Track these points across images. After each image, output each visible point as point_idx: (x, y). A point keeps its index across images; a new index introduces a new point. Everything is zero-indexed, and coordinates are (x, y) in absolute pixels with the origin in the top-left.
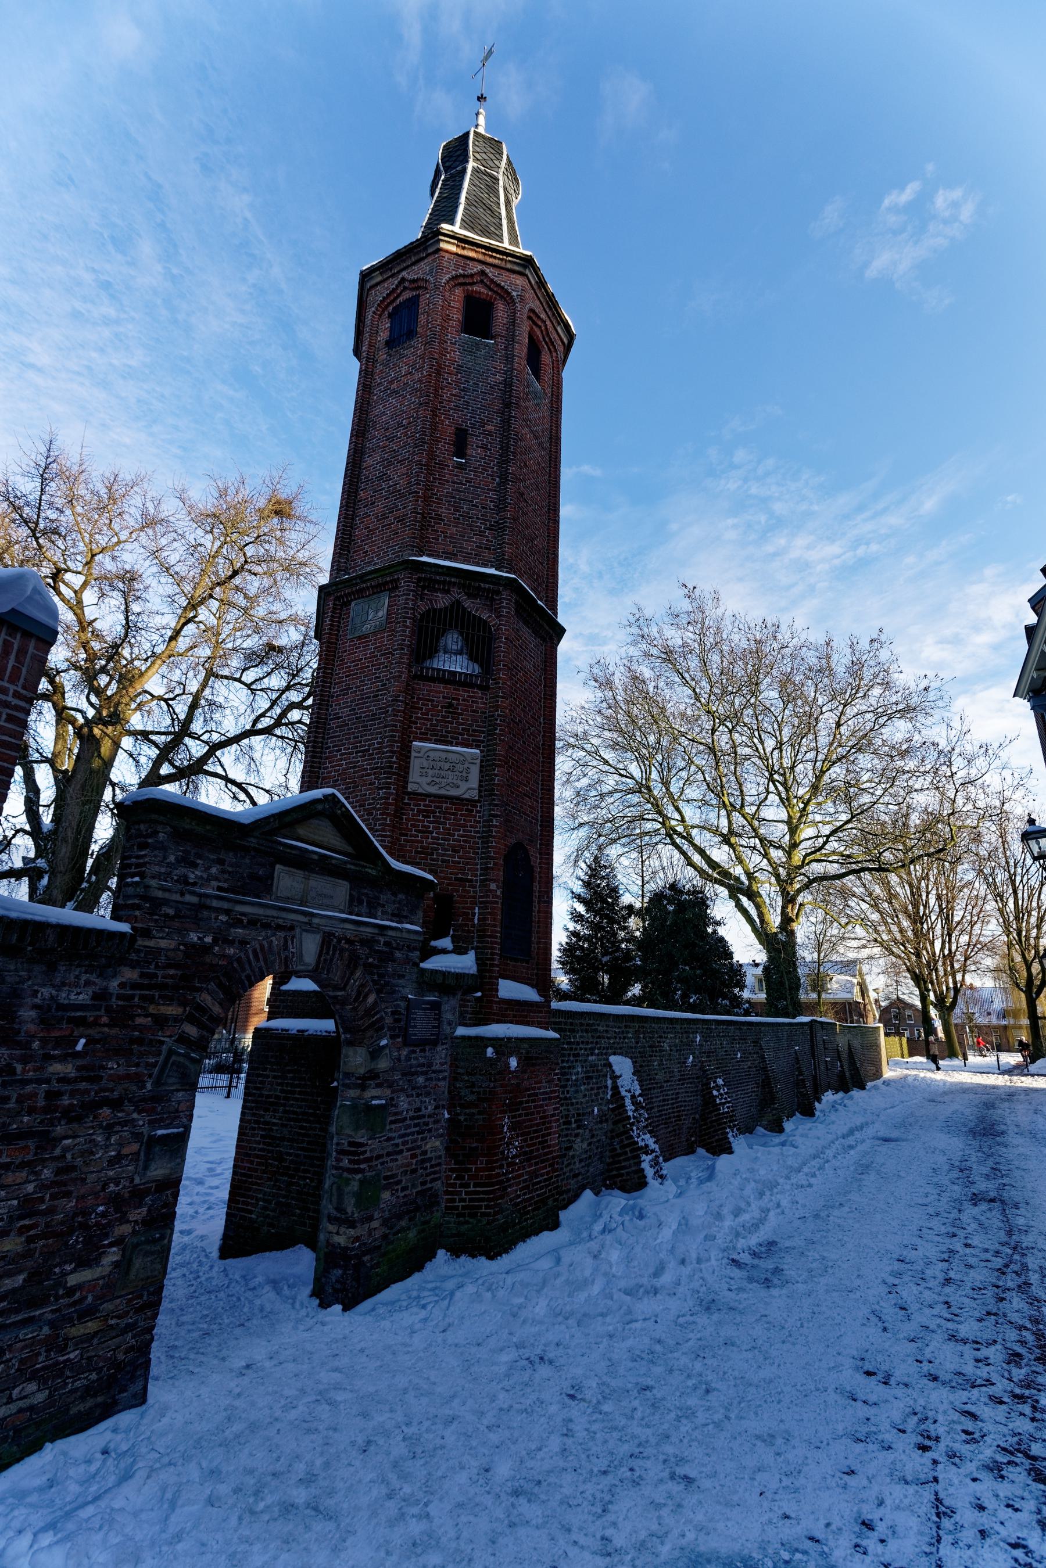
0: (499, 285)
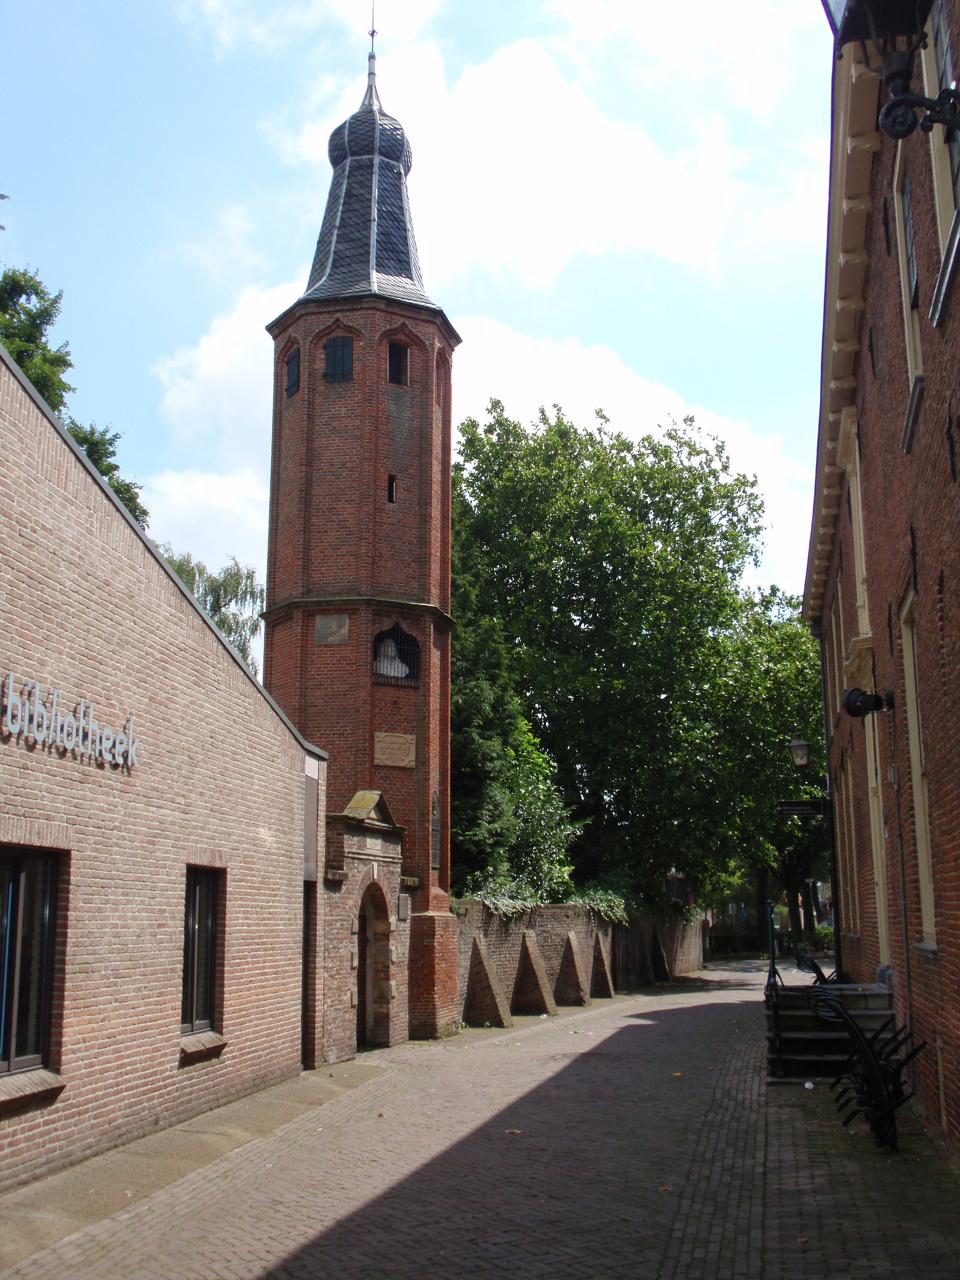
0: (416, 336)
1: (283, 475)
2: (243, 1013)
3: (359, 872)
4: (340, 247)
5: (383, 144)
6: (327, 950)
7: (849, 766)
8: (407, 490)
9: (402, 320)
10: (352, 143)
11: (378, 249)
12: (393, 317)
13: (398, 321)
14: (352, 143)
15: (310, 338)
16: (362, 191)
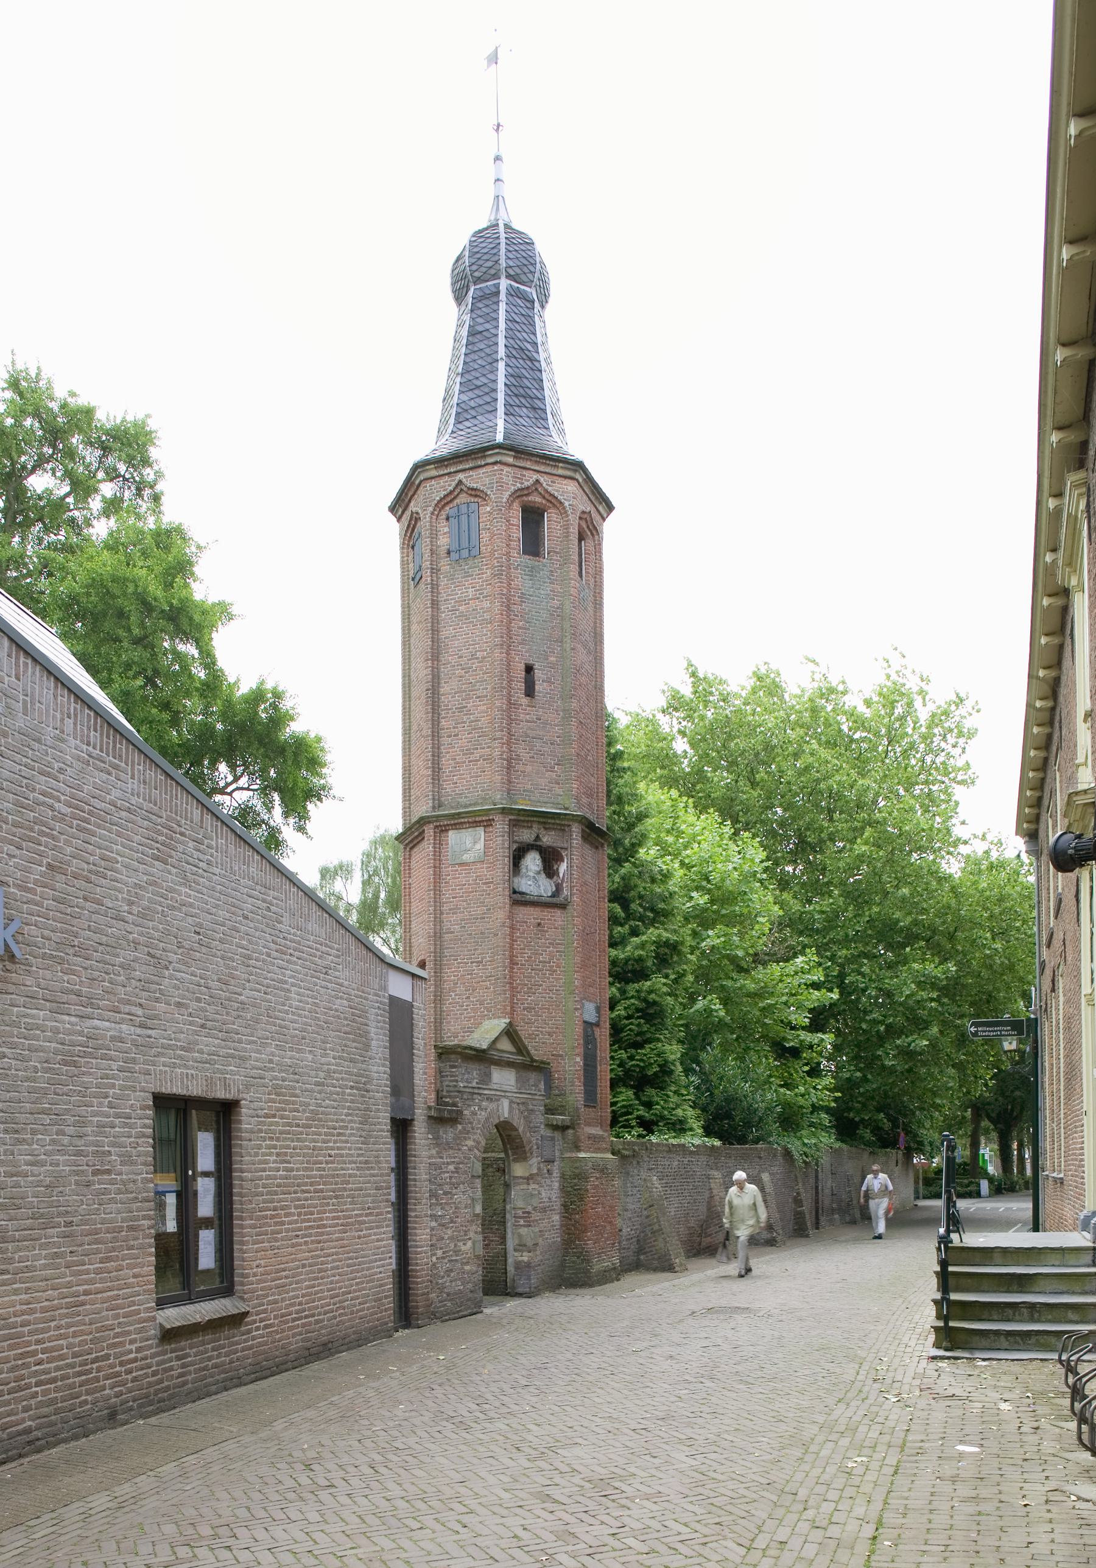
1: (413, 676)
2: (284, 1273)
3: (480, 1109)
4: (464, 397)
5: (511, 263)
6: (433, 1195)
7: (1061, 986)
8: (548, 681)
9: (535, 476)
10: (474, 268)
11: (506, 394)
12: (524, 472)
13: (530, 478)
14: (474, 268)
15: (431, 509)
16: (487, 326)
